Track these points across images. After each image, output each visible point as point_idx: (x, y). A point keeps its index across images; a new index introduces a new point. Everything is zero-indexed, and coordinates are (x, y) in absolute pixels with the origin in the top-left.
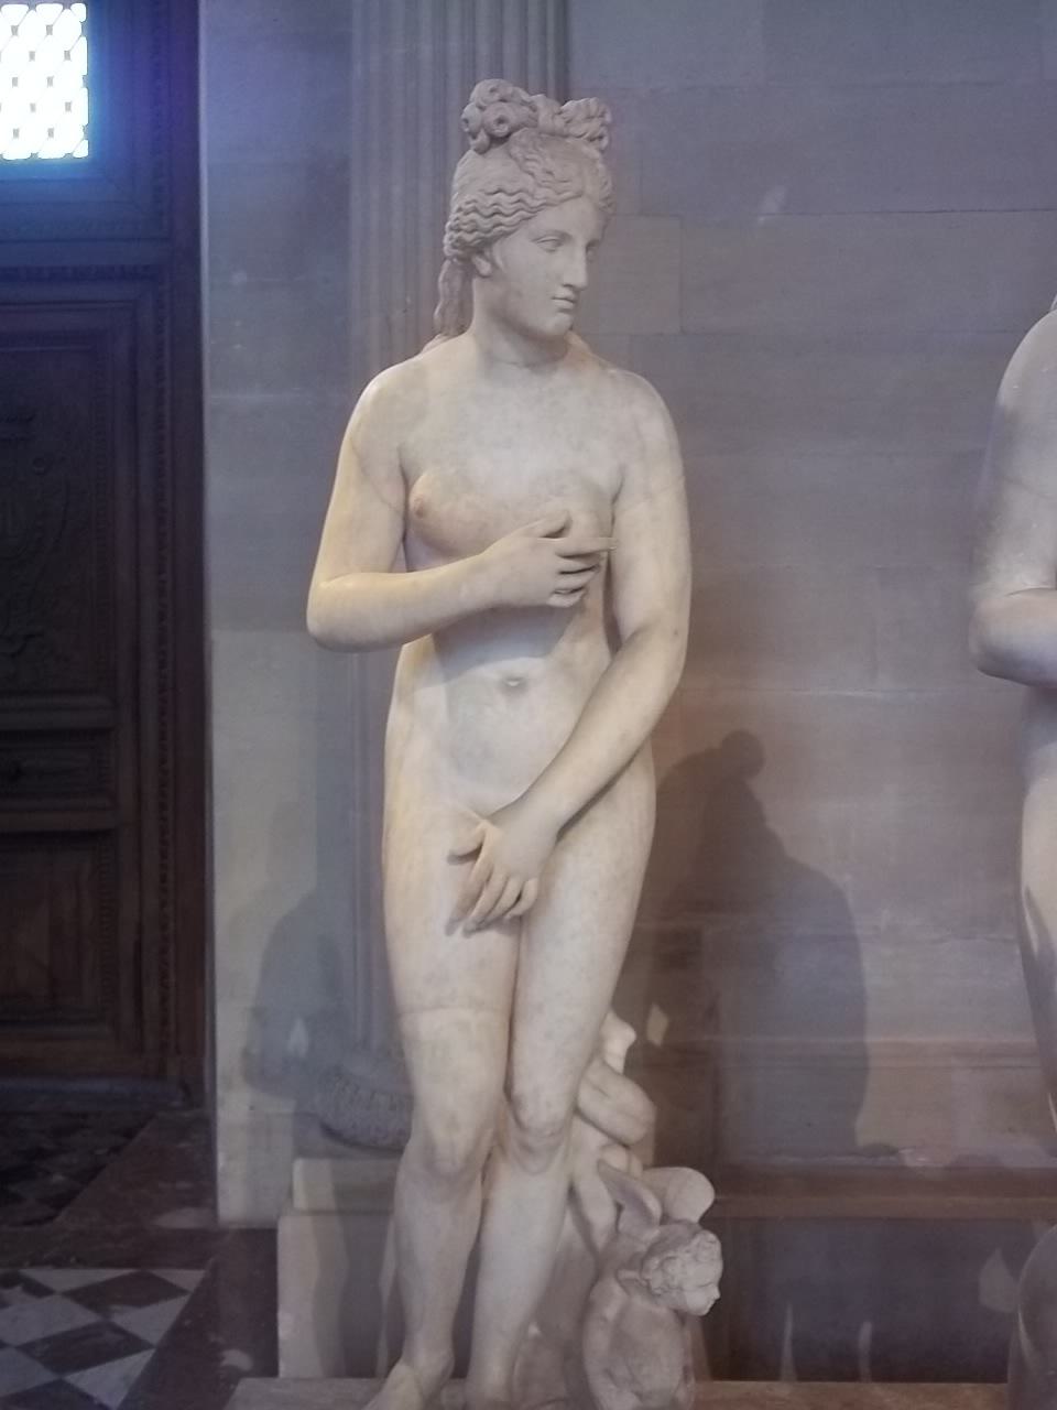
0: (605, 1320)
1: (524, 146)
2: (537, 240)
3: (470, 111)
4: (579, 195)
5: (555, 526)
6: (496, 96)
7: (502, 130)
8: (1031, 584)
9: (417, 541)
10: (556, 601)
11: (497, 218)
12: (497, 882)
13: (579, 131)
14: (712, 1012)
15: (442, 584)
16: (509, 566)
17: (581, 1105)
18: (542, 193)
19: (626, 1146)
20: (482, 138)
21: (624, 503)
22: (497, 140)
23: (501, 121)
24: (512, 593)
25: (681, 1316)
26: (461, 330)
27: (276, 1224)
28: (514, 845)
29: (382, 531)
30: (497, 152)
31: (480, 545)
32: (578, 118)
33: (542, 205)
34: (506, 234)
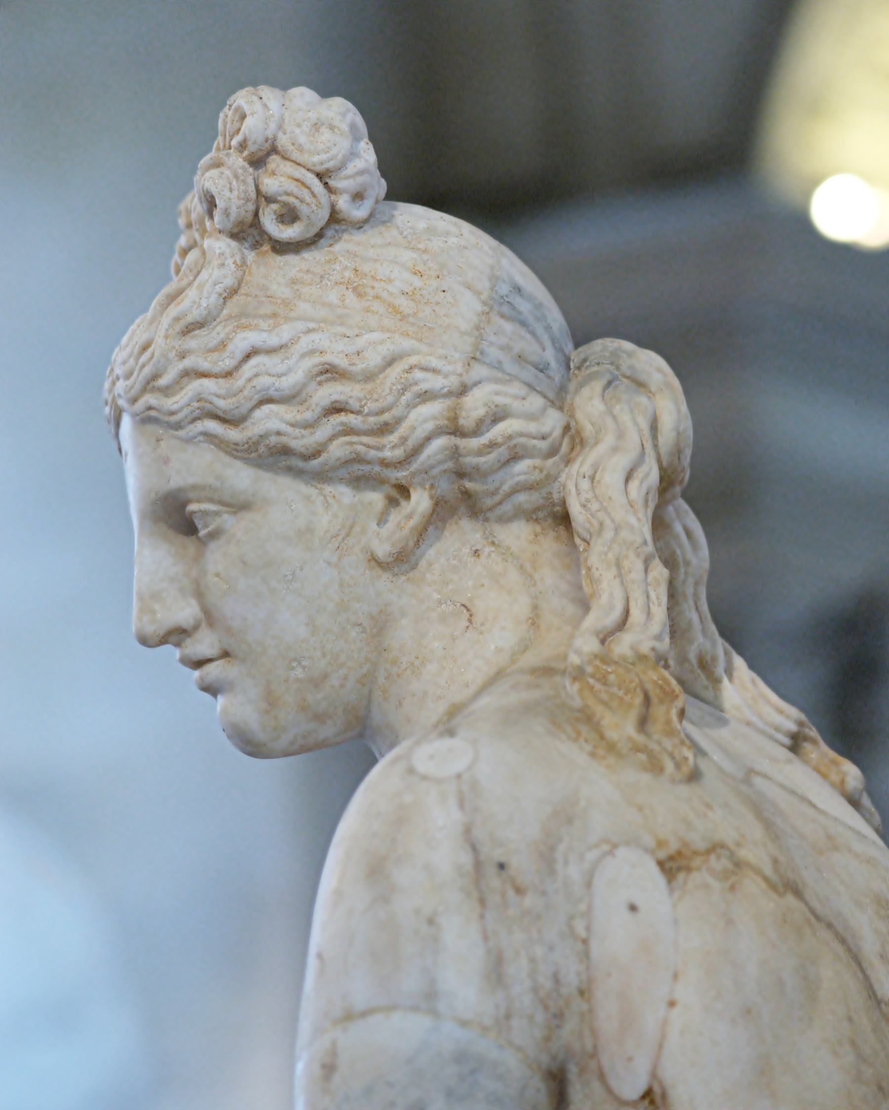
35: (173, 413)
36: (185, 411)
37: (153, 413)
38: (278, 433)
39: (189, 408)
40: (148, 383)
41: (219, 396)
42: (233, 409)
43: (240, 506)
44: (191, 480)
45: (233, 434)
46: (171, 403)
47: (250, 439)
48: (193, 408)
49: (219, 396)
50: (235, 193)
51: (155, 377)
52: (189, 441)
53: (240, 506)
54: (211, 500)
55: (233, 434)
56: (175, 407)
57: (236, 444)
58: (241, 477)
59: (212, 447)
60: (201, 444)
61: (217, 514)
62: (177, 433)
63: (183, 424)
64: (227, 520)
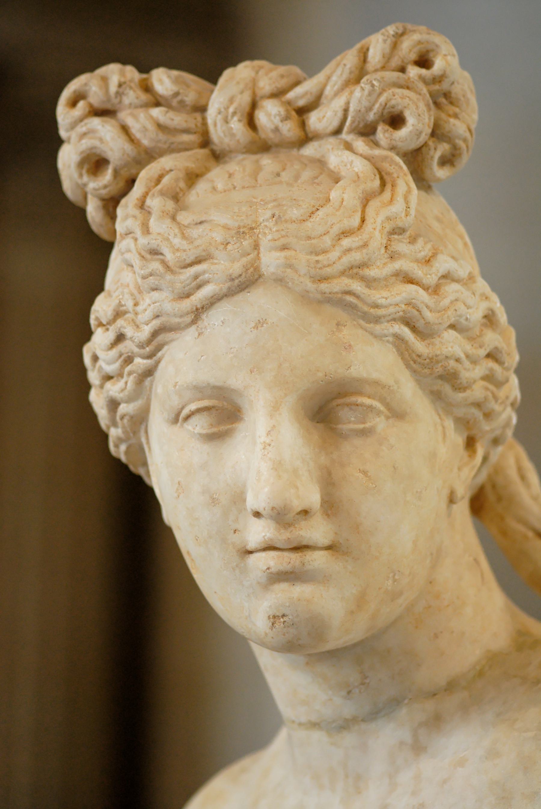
4: (245, 282)
32: (328, 91)
33: (155, 334)
35: (377, 306)
36: (392, 310)
37: (350, 299)
38: (458, 360)
39: (397, 308)
40: (351, 268)
41: (427, 307)
42: (436, 324)
43: (397, 414)
44: (375, 375)
45: (420, 346)
46: (379, 296)
47: (437, 356)
48: (400, 309)
49: (427, 307)
50: (399, 100)
51: (363, 265)
52: (379, 337)
53: (397, 414)
54: (382, 400)
55: (420, 346)
56: (383, 301)
57: (419, 356)
58: (408, 390)
59: (394, 350)
60: (388, 345)
61: (379, 413)
62: (368, 325)
63: (382, 320)
64: (380, 423)
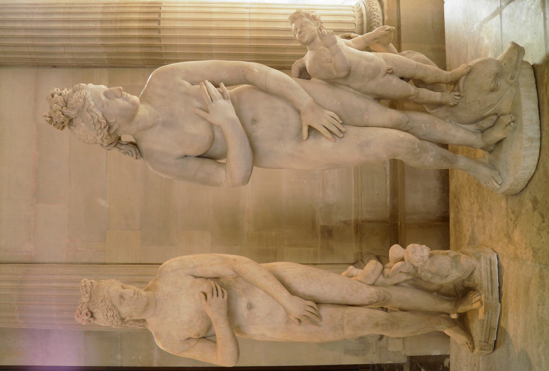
0: (431, 278)
1: (94, 308)
2: (121, 304)
3: (84, 323)
5: (203, 296)
6: (80, 316)
7: (90, 315)
8: (224, 172)
9: (207, 337)
10: (226, 297)
11: (114, 316)
12: (307, 314)
13: (90, 289)
14: (345, 222)
15: (221, 329)
16: (216, 312)
17: (372, 283)
18: (108, 303)
19: (384, 268)
20: (91, 319)
21: (196, 274)
22: (92, 316)
23: (87, 315)
24: (224, 311)
25: (431, 256)
26: (144, 320)
27: (408, 356)
28: (296, 307)
29: (205, 346)
30: (95, 315)
31: (208, 318)
34: (119, 313)
